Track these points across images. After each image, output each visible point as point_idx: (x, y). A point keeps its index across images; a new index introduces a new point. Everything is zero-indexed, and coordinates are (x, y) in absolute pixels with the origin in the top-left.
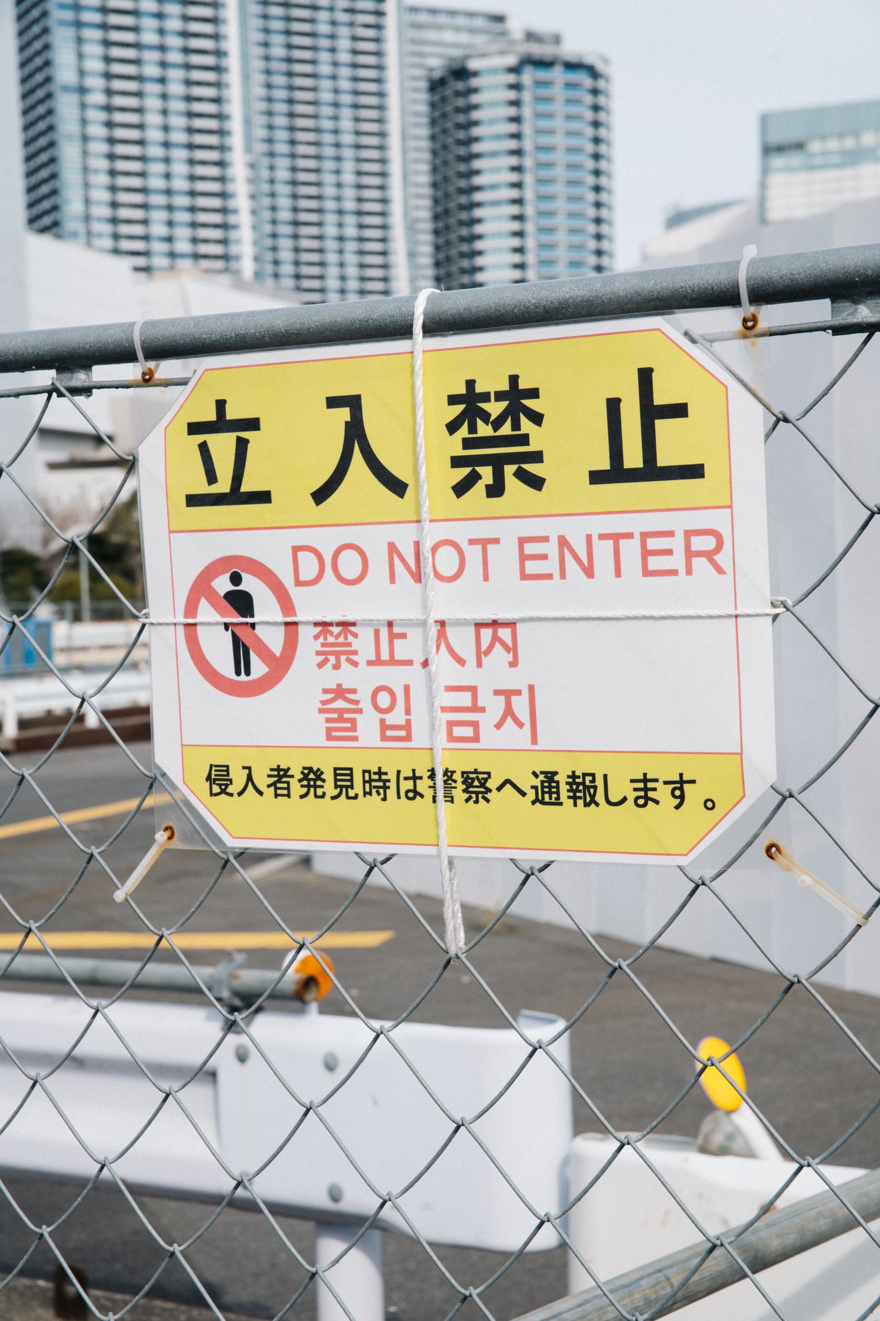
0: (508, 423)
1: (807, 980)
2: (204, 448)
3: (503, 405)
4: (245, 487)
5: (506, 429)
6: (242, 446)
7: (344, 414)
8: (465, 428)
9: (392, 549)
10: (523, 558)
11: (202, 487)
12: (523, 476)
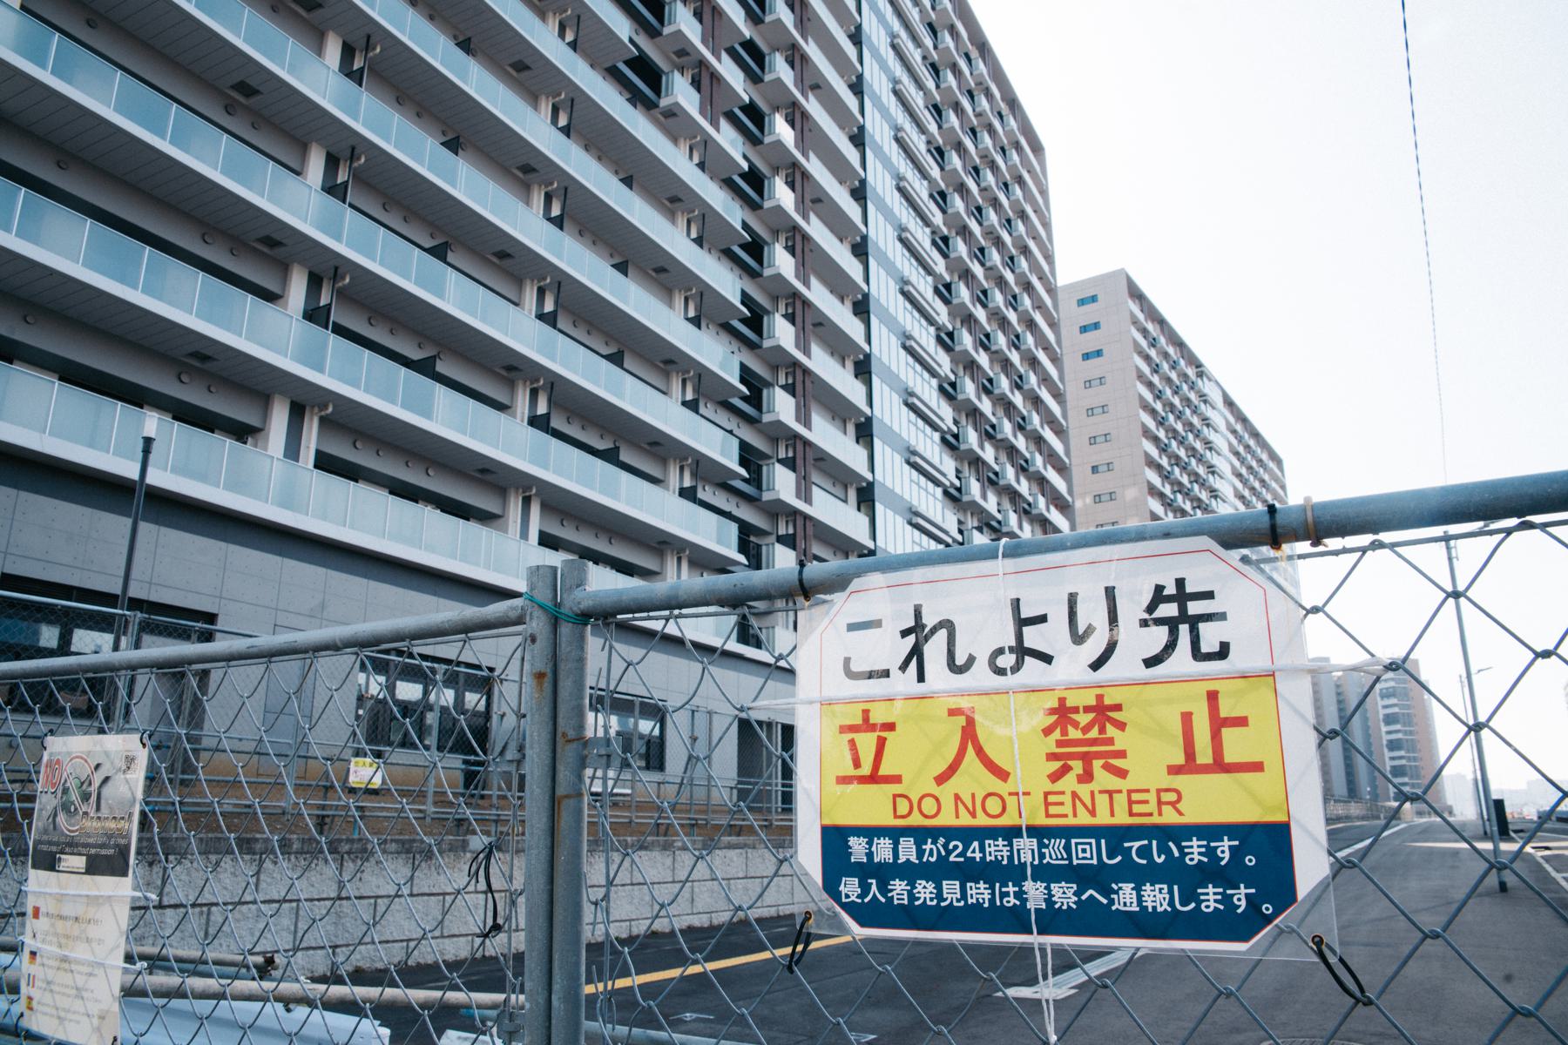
0: (1096, 729)
1: (896, 816)
2: (852, 743)
3: (1091, 716)
4: (882, 772)
5: (1094, 733)
6: (881, 743)
7: (962, 721)
8: (1058, 731)
9: (957, 797)
10: (1047, 804)
11: (851, 772)
12: (1108, 768)
